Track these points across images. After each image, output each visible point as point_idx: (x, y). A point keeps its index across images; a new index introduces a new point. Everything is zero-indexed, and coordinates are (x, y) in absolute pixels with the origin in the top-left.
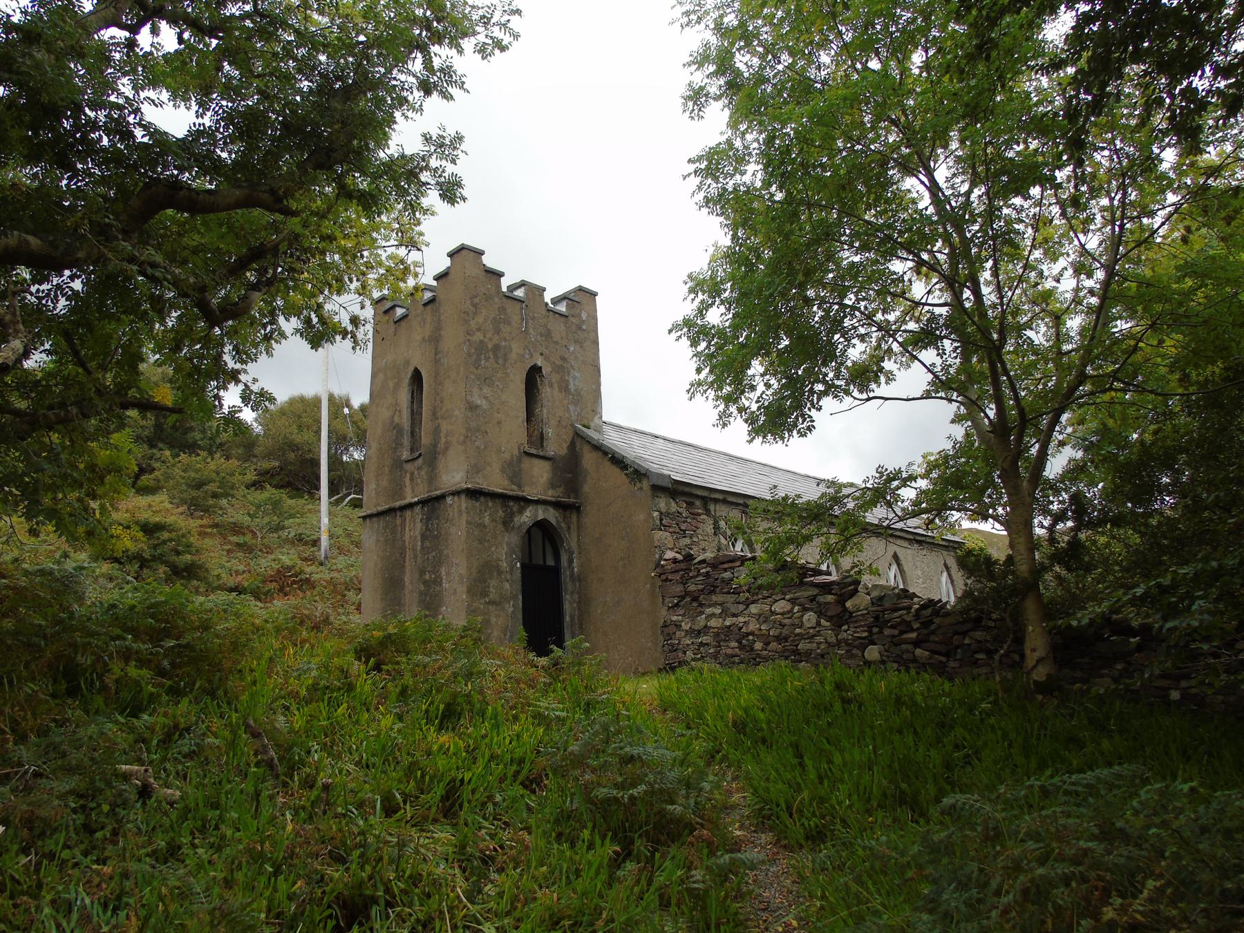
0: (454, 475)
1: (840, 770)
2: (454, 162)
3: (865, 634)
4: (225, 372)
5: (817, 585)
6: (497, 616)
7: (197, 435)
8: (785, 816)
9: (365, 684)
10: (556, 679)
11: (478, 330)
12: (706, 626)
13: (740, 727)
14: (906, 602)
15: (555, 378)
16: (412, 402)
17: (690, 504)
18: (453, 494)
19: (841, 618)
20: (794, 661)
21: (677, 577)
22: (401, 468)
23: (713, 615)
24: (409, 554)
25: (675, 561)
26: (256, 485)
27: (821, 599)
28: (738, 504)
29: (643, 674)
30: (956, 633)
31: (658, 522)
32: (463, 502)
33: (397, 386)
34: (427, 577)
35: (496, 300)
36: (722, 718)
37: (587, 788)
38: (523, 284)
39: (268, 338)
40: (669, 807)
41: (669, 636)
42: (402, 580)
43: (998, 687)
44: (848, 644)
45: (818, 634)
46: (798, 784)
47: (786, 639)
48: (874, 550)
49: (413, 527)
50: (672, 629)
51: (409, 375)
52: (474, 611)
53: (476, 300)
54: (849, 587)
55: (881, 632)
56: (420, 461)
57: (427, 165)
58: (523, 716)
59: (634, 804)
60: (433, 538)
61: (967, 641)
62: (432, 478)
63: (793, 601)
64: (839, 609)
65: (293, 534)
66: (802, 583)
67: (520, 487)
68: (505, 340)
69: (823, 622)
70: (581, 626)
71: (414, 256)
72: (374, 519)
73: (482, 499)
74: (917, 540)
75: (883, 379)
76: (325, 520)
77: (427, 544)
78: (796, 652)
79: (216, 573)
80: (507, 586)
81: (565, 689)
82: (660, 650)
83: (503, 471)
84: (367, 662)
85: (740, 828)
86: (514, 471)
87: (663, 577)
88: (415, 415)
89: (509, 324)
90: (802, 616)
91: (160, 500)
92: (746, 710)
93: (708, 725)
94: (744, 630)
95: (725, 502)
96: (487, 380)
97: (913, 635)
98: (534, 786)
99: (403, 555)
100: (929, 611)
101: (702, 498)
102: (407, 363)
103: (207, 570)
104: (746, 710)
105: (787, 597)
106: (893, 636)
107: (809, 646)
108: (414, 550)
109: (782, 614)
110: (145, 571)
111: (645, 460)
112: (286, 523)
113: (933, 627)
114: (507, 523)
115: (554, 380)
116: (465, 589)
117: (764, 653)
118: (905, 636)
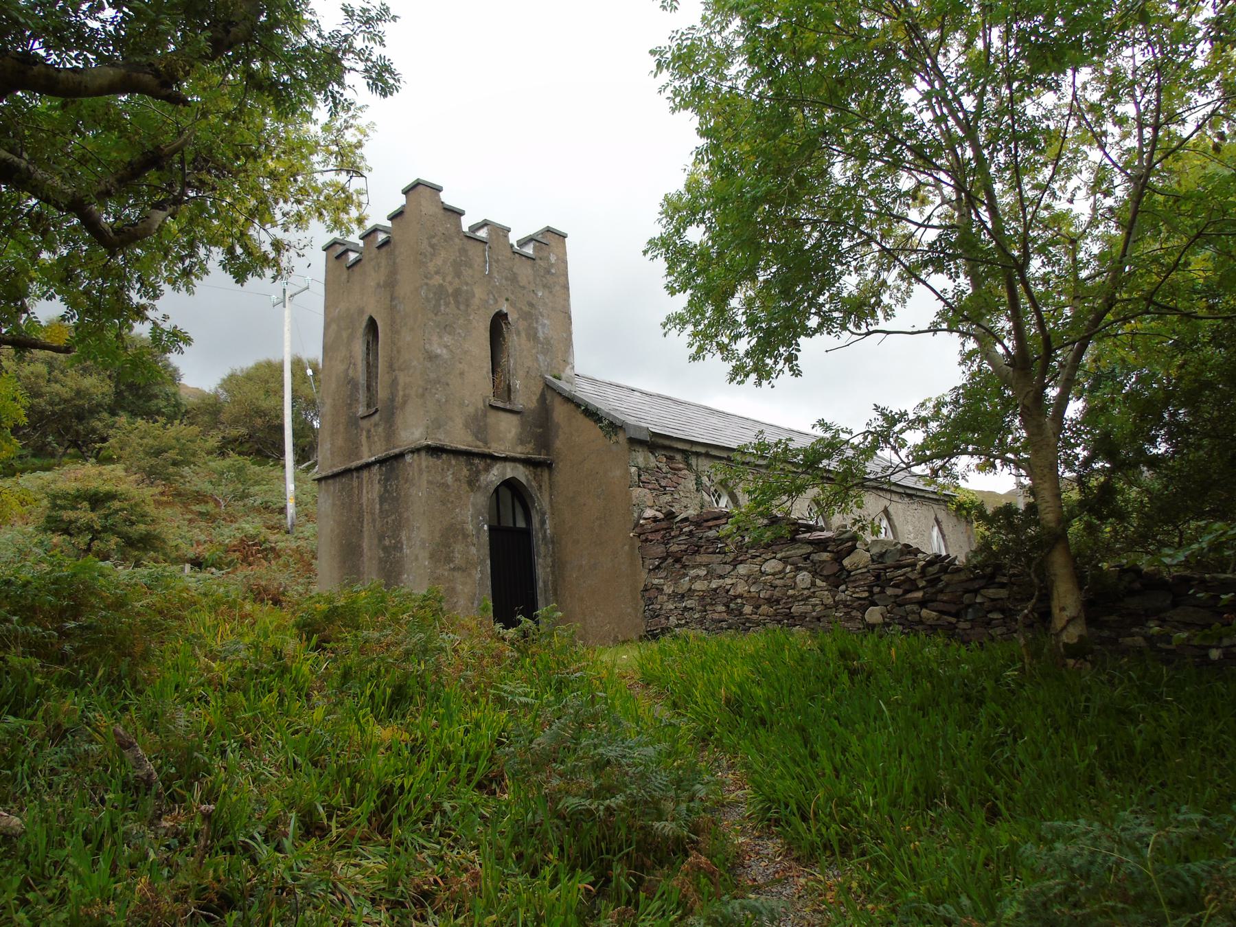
0: (412, 432)
1: (860, 760)
2: (382, 43)
3: (865, 595)
4: (129, 308)
5: (811, 542)
6: (464, 584)
7: (162, 403)
8: (796, 820)
9: (305, 663)
10: (523, 652)
11: (437, 273)
12: (690, 589)
13: (735, 705)
14: (909, 559)
15: (522, 325)
16: (368, 354)
17: (670, 459)
18: (413, 452)
19: (839, 578)
20: (788, 626)
21: (658, 536)
22: (357, 426)
23: (698, 577)
24: (367, 518)
25: (655, 519)
26: (222, 452)
27: (815, 557)
28: (720, 458)
29: (623, 642)
30: (967, 591)
31: (636, 478)
32: (425, 460)
33: (351, 338)
34: (387, 542)
35: (457, 240)
36: (713, 695)
37: (552, 799)
38: (485, 224)
39: (187, 273)
40: (657, 824)
41: (651, 601)
42: (360, 546)
43: (1024, 651)
44: (846, 606)
45: (813, 595)
46: (810, 780)
47: (778, 601)
48: (872, 504)
49: (370, 489)
50: (653, 593)
51: (364, 324)
52: (438, 578)
53: (434, 241)
54: (845, 544)
55: (882, 592)
56: (377, 417)
57: (351, 46)
58: (482, 700)
59: (611, 814)
60: (391, 499)
61: (979, 600)
62: (390, 435)
63: (785, 560)
64: (836, 568)
65: (259, 501)
66: (793, 540)
67: (486, 443)
68: (467, 284)
69: (818, 582)
70: (556, 592)
71: (356, 183)
72: (330, 481)
73: (444, 456)
74: (910, 494)
75: (880, 313)
76: (291, 487)
77: (386, 506)
78: (789, 616)
79: (174, 544)
80: (473, 550)
81: (534, 664)
82: (640, 615)
83: (467, 426)
84: (309, 639)
85: (743, 832)
86: (478, 425)
87: (643, 537)
88: (371, 368)
89: (471, 267)
90: (795, 576)
91: (118, 470)
92: (740, 686)
93: (696, 703)
94: (731, 592)
95: (707, 455)
96: (447, 328)
97: (919, 594)
98: (494, 786)
99: (360, 520)
100: (937, 567)
101: (683, 452)
102: (361, 311)
103: (164, 542)
104: (740, 686)
105: (779, 556)
106: (897, 596)
107: (803, 609)
108: (373, 514)
109: (773, 574)
110: (96, 542)
111: (622, 413)
112: (253, 490)
113: (940, 585)
114: (472, 483)
115: (521, 328)
116: (427, 555)
117: (755, 617)
118: (909, 596)
